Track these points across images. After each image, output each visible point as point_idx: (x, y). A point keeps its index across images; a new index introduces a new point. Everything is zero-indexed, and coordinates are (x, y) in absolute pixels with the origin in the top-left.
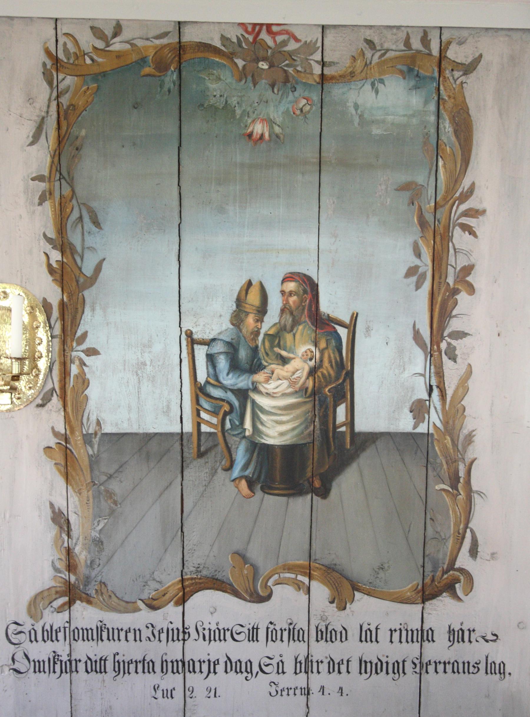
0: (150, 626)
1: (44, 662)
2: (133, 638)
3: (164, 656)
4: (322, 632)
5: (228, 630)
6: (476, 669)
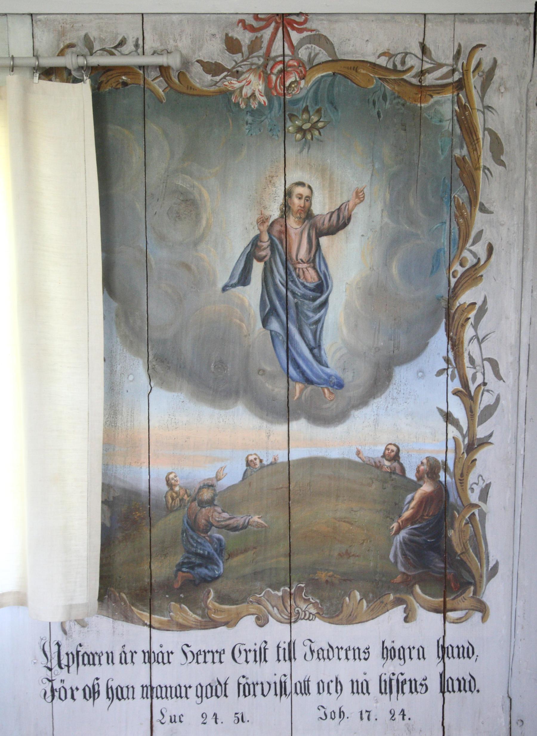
1: (275, 683)
2: (253, 659)
3: (383, 675)
5: (209, 652)
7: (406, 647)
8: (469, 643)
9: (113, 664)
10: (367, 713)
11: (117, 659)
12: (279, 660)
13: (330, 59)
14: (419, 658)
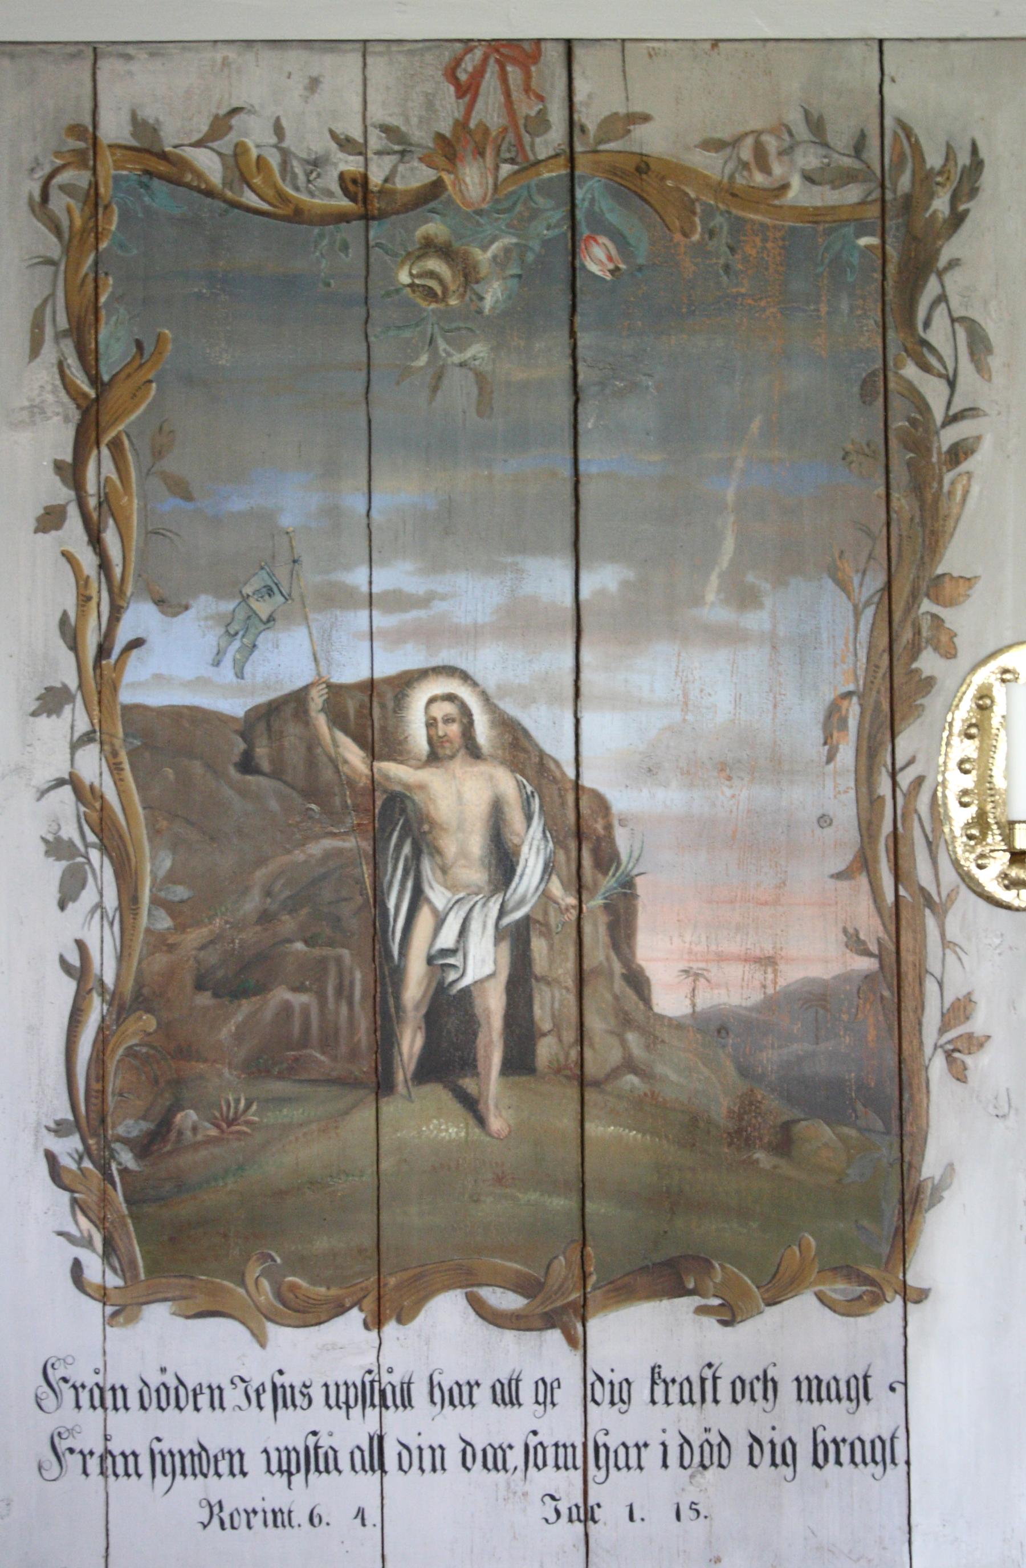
0: (237, 1380)
11: (133, 1400)
12: (800, 1399)
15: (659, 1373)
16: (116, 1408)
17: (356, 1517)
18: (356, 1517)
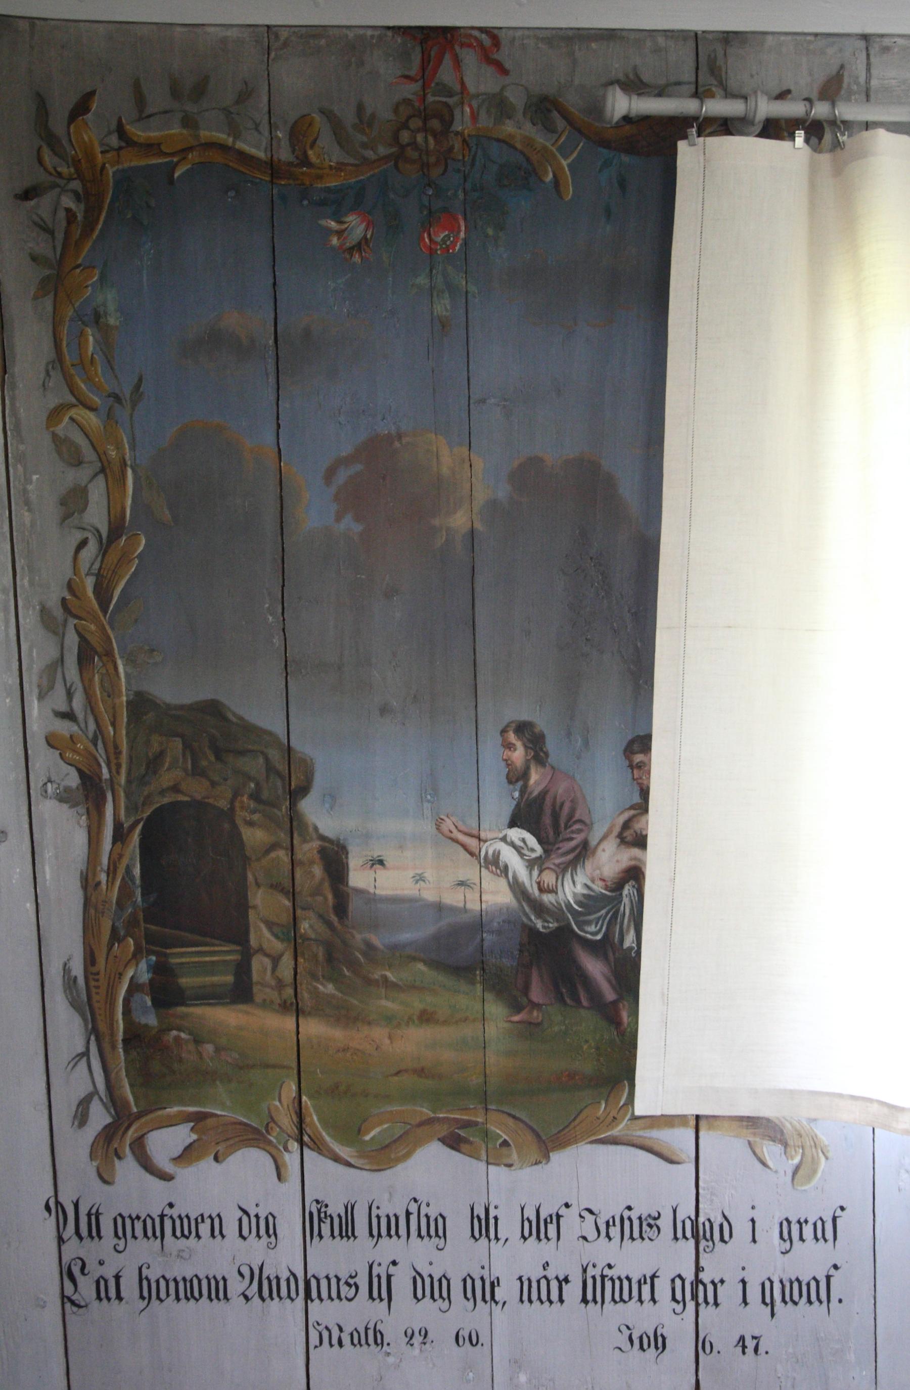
4: (530, 1222)
6: (353, 1289)
7: (793, 1220)
8: (240, 1208)
9: (223, 1236)
10: (755, 1341)
11: (231, 1228)
13: (53, 293)
14: (817, 1239)
15: (325, 1212)
16: (632, 1238)
17: (736, 1346)
18: (736, 1346)
